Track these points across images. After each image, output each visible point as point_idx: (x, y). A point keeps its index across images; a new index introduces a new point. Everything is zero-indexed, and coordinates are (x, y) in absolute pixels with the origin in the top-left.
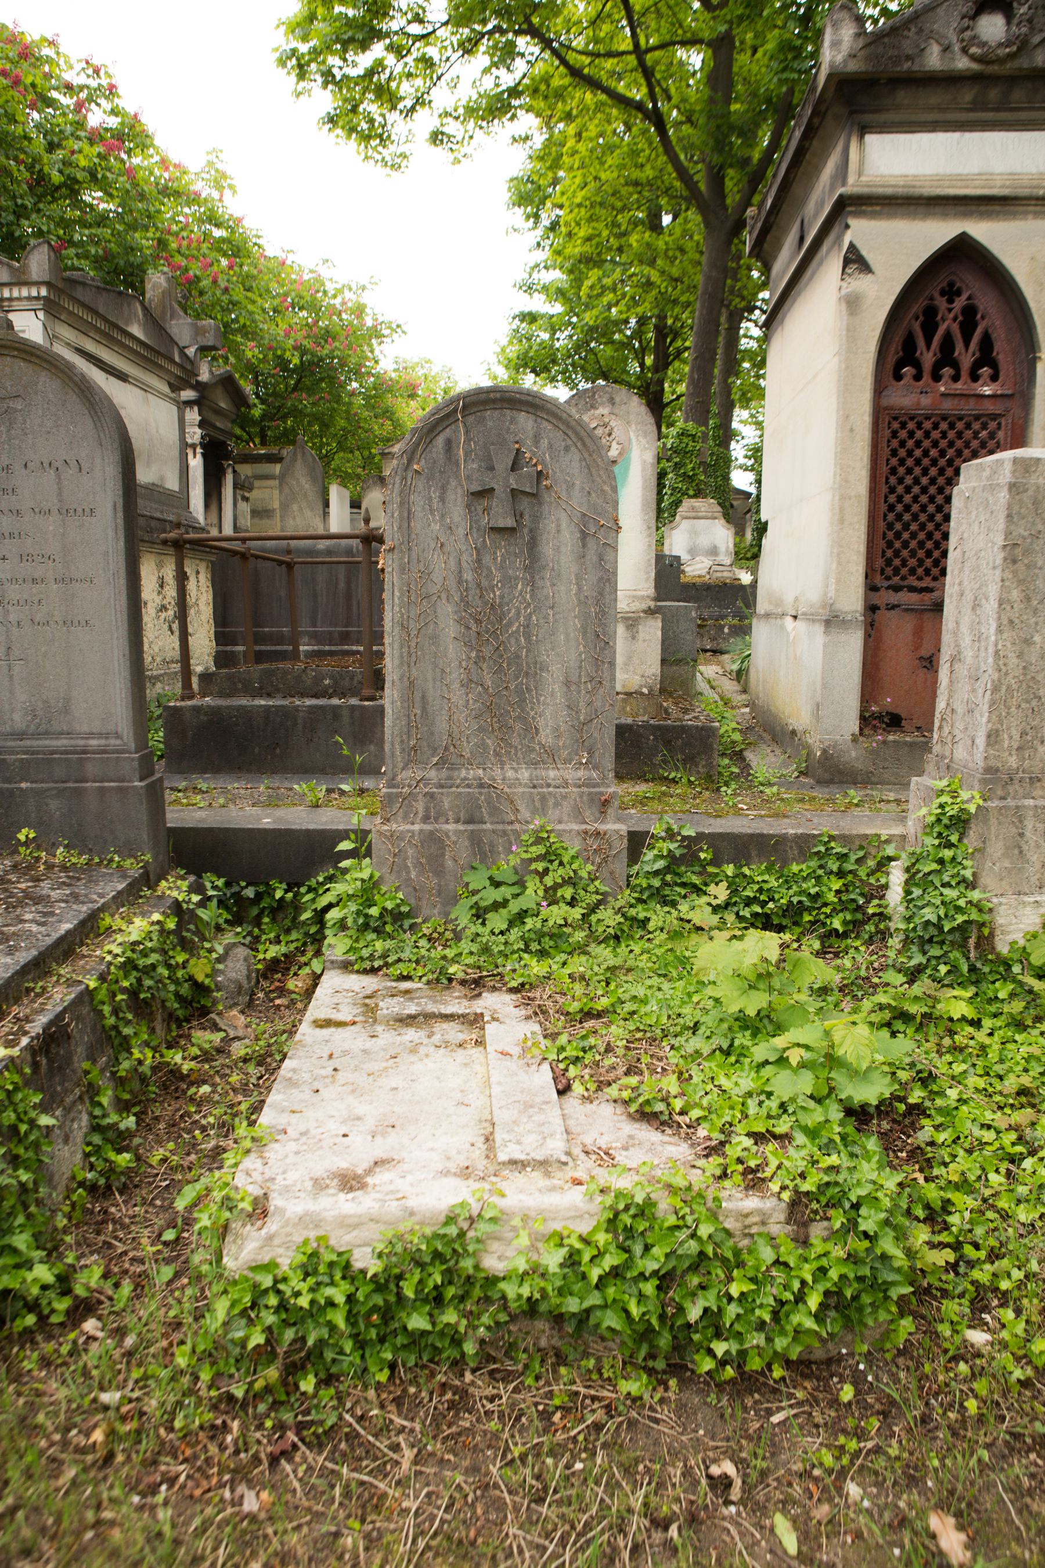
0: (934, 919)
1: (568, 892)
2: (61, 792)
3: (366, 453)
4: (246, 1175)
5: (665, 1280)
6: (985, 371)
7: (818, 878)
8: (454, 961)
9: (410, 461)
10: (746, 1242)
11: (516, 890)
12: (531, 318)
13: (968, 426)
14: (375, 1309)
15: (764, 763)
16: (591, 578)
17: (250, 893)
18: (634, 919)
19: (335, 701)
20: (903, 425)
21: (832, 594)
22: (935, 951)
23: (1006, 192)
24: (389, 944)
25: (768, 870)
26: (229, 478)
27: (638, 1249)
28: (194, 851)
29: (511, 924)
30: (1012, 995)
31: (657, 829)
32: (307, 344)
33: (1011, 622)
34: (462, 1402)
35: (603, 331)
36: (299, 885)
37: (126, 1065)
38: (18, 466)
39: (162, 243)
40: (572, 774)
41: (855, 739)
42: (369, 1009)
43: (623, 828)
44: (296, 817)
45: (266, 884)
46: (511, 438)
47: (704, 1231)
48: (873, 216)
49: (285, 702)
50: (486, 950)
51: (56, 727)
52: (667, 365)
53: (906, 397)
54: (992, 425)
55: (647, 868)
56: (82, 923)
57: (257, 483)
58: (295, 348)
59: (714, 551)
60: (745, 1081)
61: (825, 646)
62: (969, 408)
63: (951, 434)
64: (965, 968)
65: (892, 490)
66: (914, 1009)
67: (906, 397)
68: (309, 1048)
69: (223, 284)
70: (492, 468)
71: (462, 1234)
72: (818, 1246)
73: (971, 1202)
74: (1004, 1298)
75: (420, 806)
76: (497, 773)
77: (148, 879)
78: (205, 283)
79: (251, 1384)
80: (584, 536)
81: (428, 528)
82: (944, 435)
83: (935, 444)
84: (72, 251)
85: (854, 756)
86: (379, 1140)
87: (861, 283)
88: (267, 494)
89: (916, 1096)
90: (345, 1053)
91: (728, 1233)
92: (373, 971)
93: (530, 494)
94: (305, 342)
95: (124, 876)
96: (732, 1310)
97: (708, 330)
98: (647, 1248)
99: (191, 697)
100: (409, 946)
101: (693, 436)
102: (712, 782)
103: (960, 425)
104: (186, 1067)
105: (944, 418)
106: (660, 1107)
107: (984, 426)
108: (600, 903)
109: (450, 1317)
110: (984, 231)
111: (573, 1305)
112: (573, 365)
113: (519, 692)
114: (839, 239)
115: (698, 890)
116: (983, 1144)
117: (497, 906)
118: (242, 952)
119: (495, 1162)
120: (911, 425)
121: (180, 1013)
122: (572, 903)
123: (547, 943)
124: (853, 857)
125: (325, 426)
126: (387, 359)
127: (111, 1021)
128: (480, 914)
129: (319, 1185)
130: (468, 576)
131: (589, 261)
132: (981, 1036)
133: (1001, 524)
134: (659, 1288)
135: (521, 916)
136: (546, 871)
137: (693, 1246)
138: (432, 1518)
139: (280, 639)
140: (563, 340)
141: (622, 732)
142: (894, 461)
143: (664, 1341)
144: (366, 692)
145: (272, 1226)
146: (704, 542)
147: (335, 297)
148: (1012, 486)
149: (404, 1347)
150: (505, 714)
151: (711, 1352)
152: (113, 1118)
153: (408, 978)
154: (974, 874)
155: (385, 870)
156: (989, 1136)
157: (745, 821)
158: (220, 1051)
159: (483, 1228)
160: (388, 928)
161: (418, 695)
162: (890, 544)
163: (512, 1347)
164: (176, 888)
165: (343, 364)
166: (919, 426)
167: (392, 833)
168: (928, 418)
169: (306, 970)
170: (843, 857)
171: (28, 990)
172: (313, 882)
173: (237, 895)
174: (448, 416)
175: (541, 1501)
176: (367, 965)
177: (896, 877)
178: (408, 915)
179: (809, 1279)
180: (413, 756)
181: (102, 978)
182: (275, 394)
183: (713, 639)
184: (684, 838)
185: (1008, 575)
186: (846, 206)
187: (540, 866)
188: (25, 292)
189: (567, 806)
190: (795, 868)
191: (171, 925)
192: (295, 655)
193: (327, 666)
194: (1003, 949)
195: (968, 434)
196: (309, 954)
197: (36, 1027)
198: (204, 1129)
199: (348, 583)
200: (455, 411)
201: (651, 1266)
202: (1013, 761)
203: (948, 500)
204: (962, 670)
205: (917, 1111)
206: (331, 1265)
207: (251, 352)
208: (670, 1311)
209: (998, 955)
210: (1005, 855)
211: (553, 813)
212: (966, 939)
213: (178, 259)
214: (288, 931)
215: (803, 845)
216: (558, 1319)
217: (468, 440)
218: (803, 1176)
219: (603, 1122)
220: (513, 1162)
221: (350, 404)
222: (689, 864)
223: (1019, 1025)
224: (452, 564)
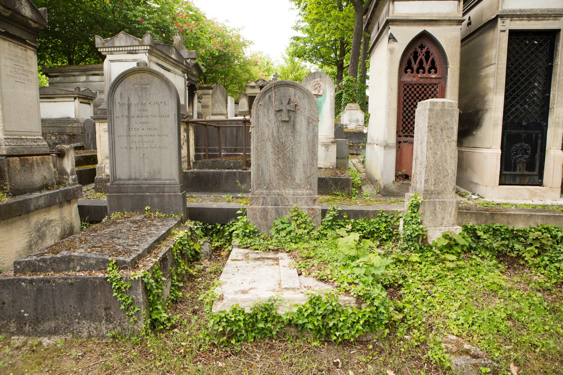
0: (410, 234)
1: (304, 226)
2: (158, 196)
3: (240, 85)
4: (217, 291)
5: (324, 316)
6: (433, 70)
7: (379, 224)
8: (270, 245)
9: (259, 102)
10: (345, 308)
11: (289, 225)
12: (297, 39)
13: (428, 87)
14: (250, 322)
15: (367, 190)
16: (311, 135)
17: (210, 227)
18: (323, 234)
19: (234, 170)
20: (408, 87)
21: (386, 138)
22: (410, 243)
23: (437, 18)
24: (252, 240)
25: (364, 221)
26: (196, 97)
27: (317, 308)
28: (194, 214)
29: (287, 234)
30: (432, 256)
31: (330, 208)
32: (221, 49)
33: (431, 148)
34: (272, 347)
35: (323, 44)
36: (224, 225)
37: (180, 270)
38: (148, 104)
39: (174, 19)
40: (305, 192)
41: (394, 183)
42: (246, 257)
43: (320, 208)
44: (224, 205)
45: (215, 224)
46: (288, 95)
47: (334, 304)
48: (397, 25)
49: (219, 171)
50: (280, 242)
51: (157, 177)
52: (344, 55)
53: (409, 78)
54: (435, 87)
55: (327, 219)
56: (167, 231)
57: (204, 96)
58: (217, 50)
59: (357, 121)
60: (348, 271)
61: (384, 154)
62: (428, 81)
63: (423, 90)
64: (418, 248)
65: (405, 106)
66: (403, 259)
67: (409, 78)
68: (230, 266)
69: (194, 31)
70: (282, 104)
71: (272, 304)
72: (364, 309)
73: (411, 306)
74: (415, 328)
75: (261, 201)
76: (283, 191)
77: (182, 221)
78: (188, 31)
79: (219, 341)
80: (309, 123)
81: (264, 121)
82: (420, 90)
83: (418, 92)
84: (146, 22)
85: (394, 187)
86: (251, 284)
87: (393, 45)
88: (207, 100)
89: (401, 282)
90: (240, 267)
91: (341, 306)
92: (247, 248)
93: (293, 111)
94: (220, 48)
95: (176, 220)
96: (341, 324)
97: (358, 43)
98: (319, 308)
99: (190, 169)
100: (257, 241)
101: (352, 81)
102: (350, 195)
103: (425, 87)
104: (194, 273)
105: (420, 85)
106: (325, 277)
107: (433, 87)
108: (313, 229)
109: (269, 325)
110: (430, 29)
111: (300, 322)
112: (312, 54)
113: (290, 168)
114: (387, 31)
115: (343, 226)
116: (417, 293)
117: (283, 229)
118: (207, 244)
119: (281, 288)
120: (410, 87)
121: (191, 259)
122: (305, 229)
123: (297, 240)
124: (390, 217)
125: (226, 76)
126: (248, 53)
127: (176, 257)
128: (278, 232)
129: (236, 293)
130: (275, 134)
131: (318, 20)
132: (421, 266)
133: (427, 120)
134: (322, 318)
135: (290, 232)
136: (297, 220)
137: (331, 308)
138: (265, 369)
139: (215, 151)
140: (309, 46)
141: (320, 180)
142: (405, 98)
143: (324, 332)
144: (244, 168)
145: (224, 301)
146: (354, 118)
147: (230, 32)
148: (430, 110)
149: (257, 333)
150: (286, 175)
151: (335, 335)
152: (177, 283)
153: (257, 249)
154: (421, 221)
155: (251, 219)
156: (419, 291)
157: (358, 207)
158: (203, 270)
159: (278, 302)
160: (252, 236)
161: (260, 169)
162: (404, 123)
163: (285, 334)
164: (190, 224)
165: (233, 55)
166: (413, 87)
167: (253, 208)
168: (415, 85)
169: (227, 249)
170: (387, 217)
171: (156, 247)
172: (229, 224)
173: (206, 228)
174: (269, 89)
175: (292, 366)
176: (245, 246)
177: (401, 222)
178: (257, 232)
179: (361, 317)
180: (259, 186)
181: (174, 245)
182: (209, 65)
183: (356, 150)
184: (338, 211)
185: (429, 134)
186: (388, 22)
187: (296, 218)
188: (143, 48)
189: (303, 201)
190: (372, 220)
191: (189, 234)
192: (220, 156)
193: (232, 160)
194: (430, 243)
195: (428, 89)
196: (227, 245)
197: (161, 255)
198: (200, 289)
199: (237, 132)
200: (272, 87)
201: (320, 312)
202: (433, 188)
203: (414, 112)
204: (418, 161)
205: (401, 286)
206: (240, 311)
207: (202, 52)
208: (325, 324)
209: (429, 245)
210: (431, 215)
211: (300, 203)
212: (418, 240)
213: (180, 24)
214: (221, 238)
215: (375, 214)
216: (297, 325)
217: (275, 96)
218: (360, 292)
219: (311, 281)
220: (286, 288)
221: (235, 68)
222: (339, 219)
223: (434, 264)
224: (271, 131)
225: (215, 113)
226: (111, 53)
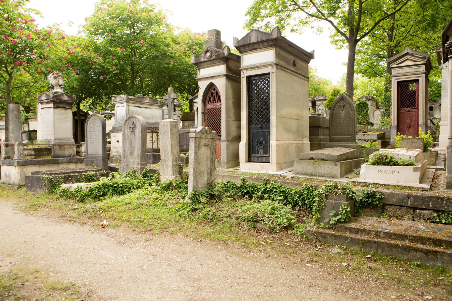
6: (219, 101)
225: (296, 121)
226: (116, 103)
